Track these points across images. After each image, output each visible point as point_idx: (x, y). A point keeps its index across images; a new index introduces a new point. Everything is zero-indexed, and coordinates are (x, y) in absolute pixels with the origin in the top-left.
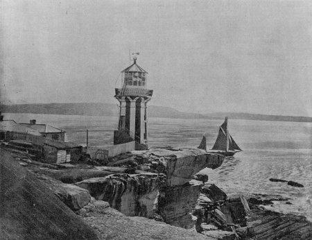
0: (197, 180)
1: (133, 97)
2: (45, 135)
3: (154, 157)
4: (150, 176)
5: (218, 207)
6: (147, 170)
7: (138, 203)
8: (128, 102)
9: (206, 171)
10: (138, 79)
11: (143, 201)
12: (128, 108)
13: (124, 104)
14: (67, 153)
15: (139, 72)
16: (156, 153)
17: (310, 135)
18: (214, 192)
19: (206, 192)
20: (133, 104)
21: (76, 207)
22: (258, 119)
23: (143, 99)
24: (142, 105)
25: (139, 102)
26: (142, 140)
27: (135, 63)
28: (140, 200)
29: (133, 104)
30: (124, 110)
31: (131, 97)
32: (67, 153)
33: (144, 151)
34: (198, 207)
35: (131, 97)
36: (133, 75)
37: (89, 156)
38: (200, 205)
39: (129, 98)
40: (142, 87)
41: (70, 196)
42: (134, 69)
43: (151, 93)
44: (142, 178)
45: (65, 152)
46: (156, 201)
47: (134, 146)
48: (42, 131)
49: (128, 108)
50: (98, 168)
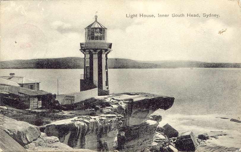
0: (152, 120)
1: (95, 50)
2: (22, 85)
3: (114, 101)
4: (110, 117)
5: (172, 143)
6: (108, 113)
7: (100, 142)
8: (90, 53)
9: (159, 112)
10: (99, 35)
11: (103, 140)
12: (91, 58)
13: (88, 56)
14: (39, 100)
15: (100, 29)
16: (115, 98)
17: (4, 1)
18: (169, 131)
19: (160, 130)
20: (95, 56)
21: (25, 142)
22: (210, 67)
23: (103, 51)
24: (104, 56)
25: (100, 54)
26: (104, 88)
27: (96, 21)
28: (101, 139)
29: (95, 56)
30: (88, 60)
31: (93, 49)
32: (39, 100)
33: (106, 96)
34: (154, 144)
35: (93, 49)
36: (95, 32)
37: (58, 102)
38: (156, 142)
39: (92, 51)
40: (102, 41)
41: (19, 132)
42: (96, 26)
43: (110, 46)
44: (102, 120)
45: (36, 100)
46: (116, 139)
47: (97, 92)
48: (20, 82)
49: (91, 58)
50: (65, 112)
